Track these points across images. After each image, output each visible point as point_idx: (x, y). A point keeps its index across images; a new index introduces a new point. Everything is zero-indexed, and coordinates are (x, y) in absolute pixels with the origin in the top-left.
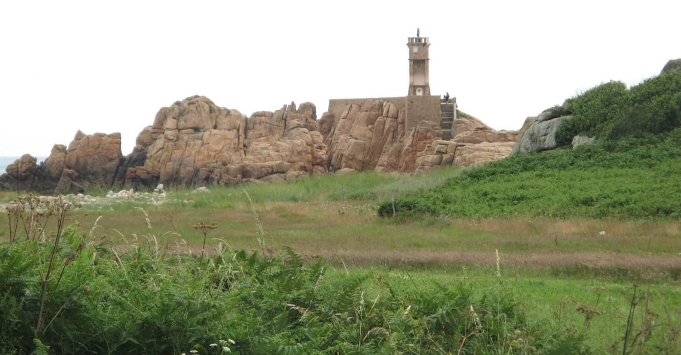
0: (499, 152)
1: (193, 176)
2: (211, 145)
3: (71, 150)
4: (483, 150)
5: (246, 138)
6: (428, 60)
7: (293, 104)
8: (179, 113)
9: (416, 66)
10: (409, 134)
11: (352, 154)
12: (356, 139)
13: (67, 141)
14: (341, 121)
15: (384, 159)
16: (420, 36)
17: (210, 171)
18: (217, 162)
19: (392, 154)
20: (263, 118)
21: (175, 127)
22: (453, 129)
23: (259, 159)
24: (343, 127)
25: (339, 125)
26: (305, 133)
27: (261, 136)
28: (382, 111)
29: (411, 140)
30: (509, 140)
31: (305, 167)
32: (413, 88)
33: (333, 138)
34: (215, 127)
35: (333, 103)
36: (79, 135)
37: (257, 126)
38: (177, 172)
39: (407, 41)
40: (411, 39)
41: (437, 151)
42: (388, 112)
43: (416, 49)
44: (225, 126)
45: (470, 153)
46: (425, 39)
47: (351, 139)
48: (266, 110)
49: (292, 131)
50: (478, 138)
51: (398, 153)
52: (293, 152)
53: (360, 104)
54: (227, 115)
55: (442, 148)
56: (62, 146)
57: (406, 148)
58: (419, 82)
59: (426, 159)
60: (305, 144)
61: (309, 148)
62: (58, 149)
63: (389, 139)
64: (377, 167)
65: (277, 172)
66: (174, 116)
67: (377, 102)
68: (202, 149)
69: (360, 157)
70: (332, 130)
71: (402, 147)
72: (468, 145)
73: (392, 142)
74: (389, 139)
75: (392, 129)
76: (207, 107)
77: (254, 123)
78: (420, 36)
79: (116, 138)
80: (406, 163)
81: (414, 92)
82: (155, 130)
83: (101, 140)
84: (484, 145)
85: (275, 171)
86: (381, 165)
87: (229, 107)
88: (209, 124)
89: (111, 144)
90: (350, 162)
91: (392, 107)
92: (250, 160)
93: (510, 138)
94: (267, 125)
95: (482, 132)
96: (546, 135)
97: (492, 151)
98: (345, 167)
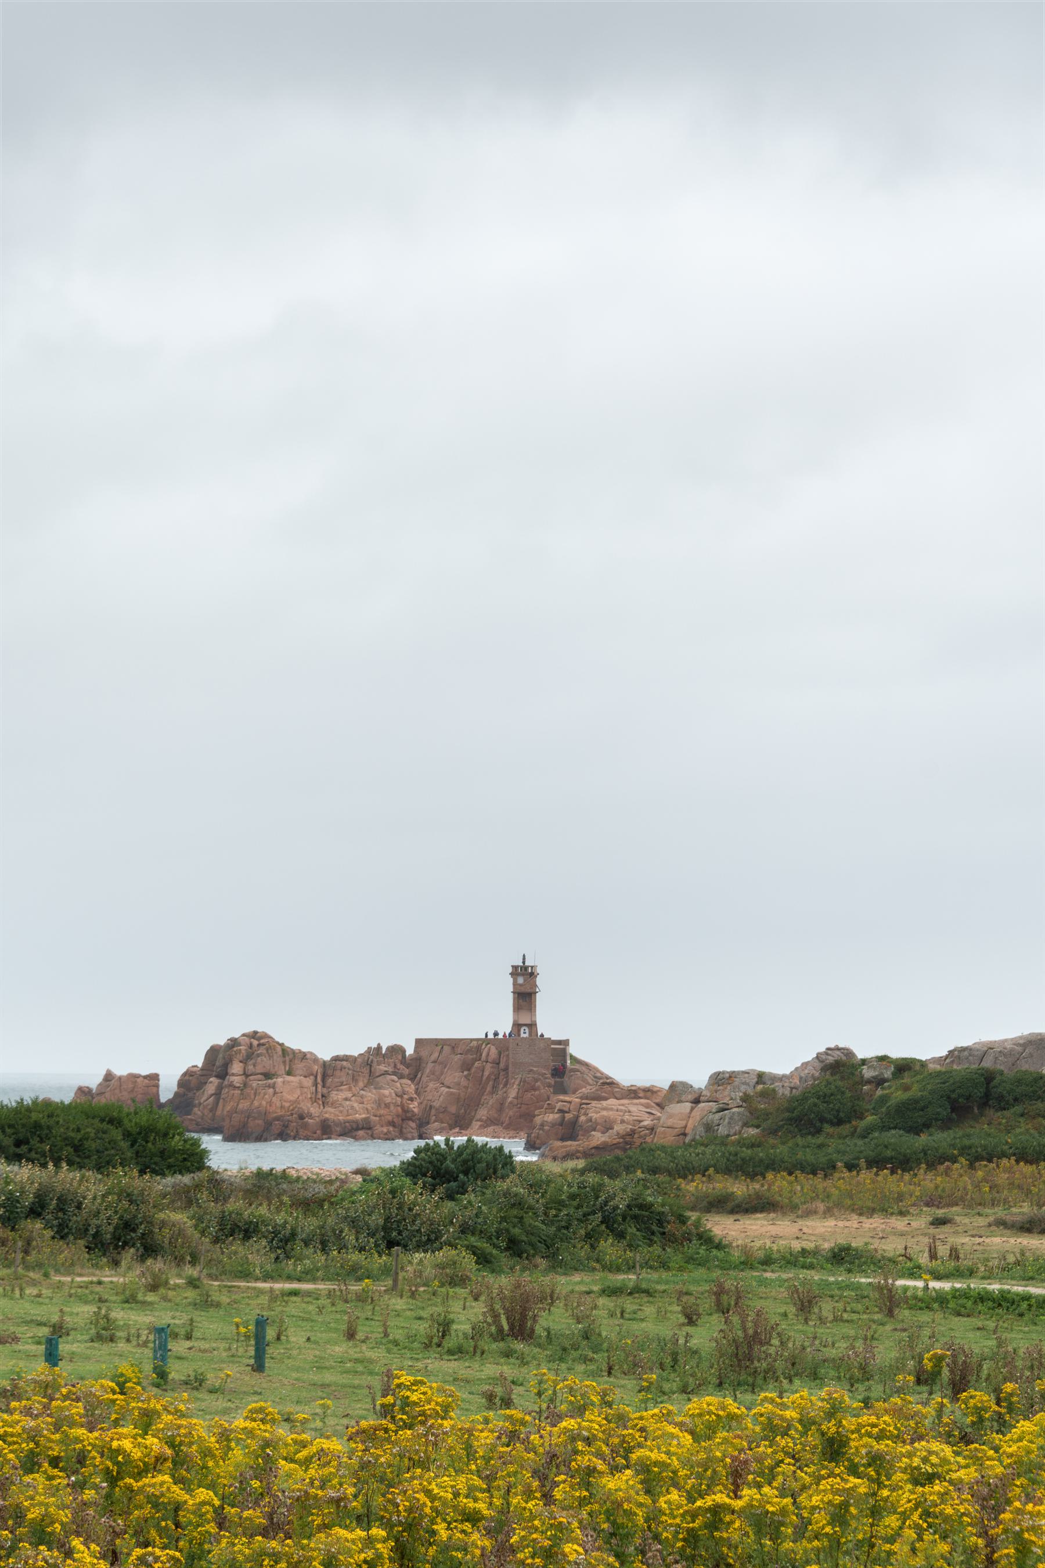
0: (629, 1112)
1: (264, 1131)
2: (284, 1094)
3: (100, 1093)
4: (612, 1109)
5: (324, 1086)
6: (536, 993)
7: (379, 1047)
8: (247, 1056)
9: (521, 1001)
10: (514, 1083)
11: (444, 1106)
12: (449, 1087)
13: (93, 1080)
14: (430, 1065)
15: (483, 1113)
16: (527, 964)
17: (284, 1126)
18: (292, 1114)
19: (492, 1106)
20: (344, 1063)
21: (242, 1073)
22: (566, 1079)
23: (341, 1112)
24: (433, 1073)
25: (428, 1071)
26: (393, 1081)
27: (342, 1084)
28: (481, 1055)
29: (517, 1090)
30: (640, 1098)
31: (393, 1122)
32: (517, 1026)
33: (420, 1085)
34: (289, 1073)
35: (419, 1043)
36: (109, 1077)
37: (338, 1073)
38: (245, 1125)
39: (510, 970)
40: (515, 967)
41: (558, 1110)
42: (488, 1055)
43: (520, 980)
44: (300, 1072)
45: (597, 1113)
46: (532, 967)
47: (443, 1088)
48: (348, 1053)
49: (378, 1079)
50: (603, 1094)
51: (501, 1107)
52: (379, 1104)
53: (453, 1044)
54: (303, 1059)
55: (564, 1106)
56: (88, 1087)
57: (510, 1100)
58: (525, 1019)
59: (546, 1119)
60: (394, 1095)
61: (399, 1099)
62: (82, 1091)
63: (489, 1089)
64: (474, 1122)
65: (362, 1128)
66: (241, 1059)
67: (475, 1043)
68: (274, 1099)
69: (453, 1109)
70: (419, 1076)
71: (505, 1099)
72: (594, 1103)
73: (492, 1093)
74: (489, 1089)
75: (493, 1077)
76: (279, 1049)
77: (335, 1069)
78: (527, 964)
79: (154, 1078)
80: (510, 1118)
81: (519, 1031)
82: (205, 1072)
83: (136, 1082)
84: (612, 1102)
85: (360, 1126)
86: (480, 1120)
87: (304, 1050)
88: (281, 1069)
89: (148, 1087)
90: (441, 1115)
91: (494, 1051)
92: (331, 1113)
93: (641, 1094)
94: (350, 1072)
95: (608, 1086)
96: (719, 1125)
97: (621, 1111)
98: (435, 1121)
